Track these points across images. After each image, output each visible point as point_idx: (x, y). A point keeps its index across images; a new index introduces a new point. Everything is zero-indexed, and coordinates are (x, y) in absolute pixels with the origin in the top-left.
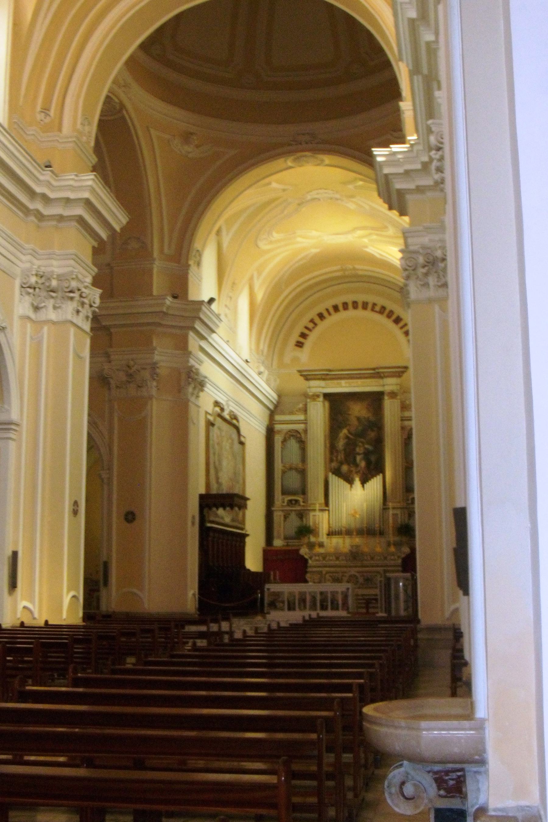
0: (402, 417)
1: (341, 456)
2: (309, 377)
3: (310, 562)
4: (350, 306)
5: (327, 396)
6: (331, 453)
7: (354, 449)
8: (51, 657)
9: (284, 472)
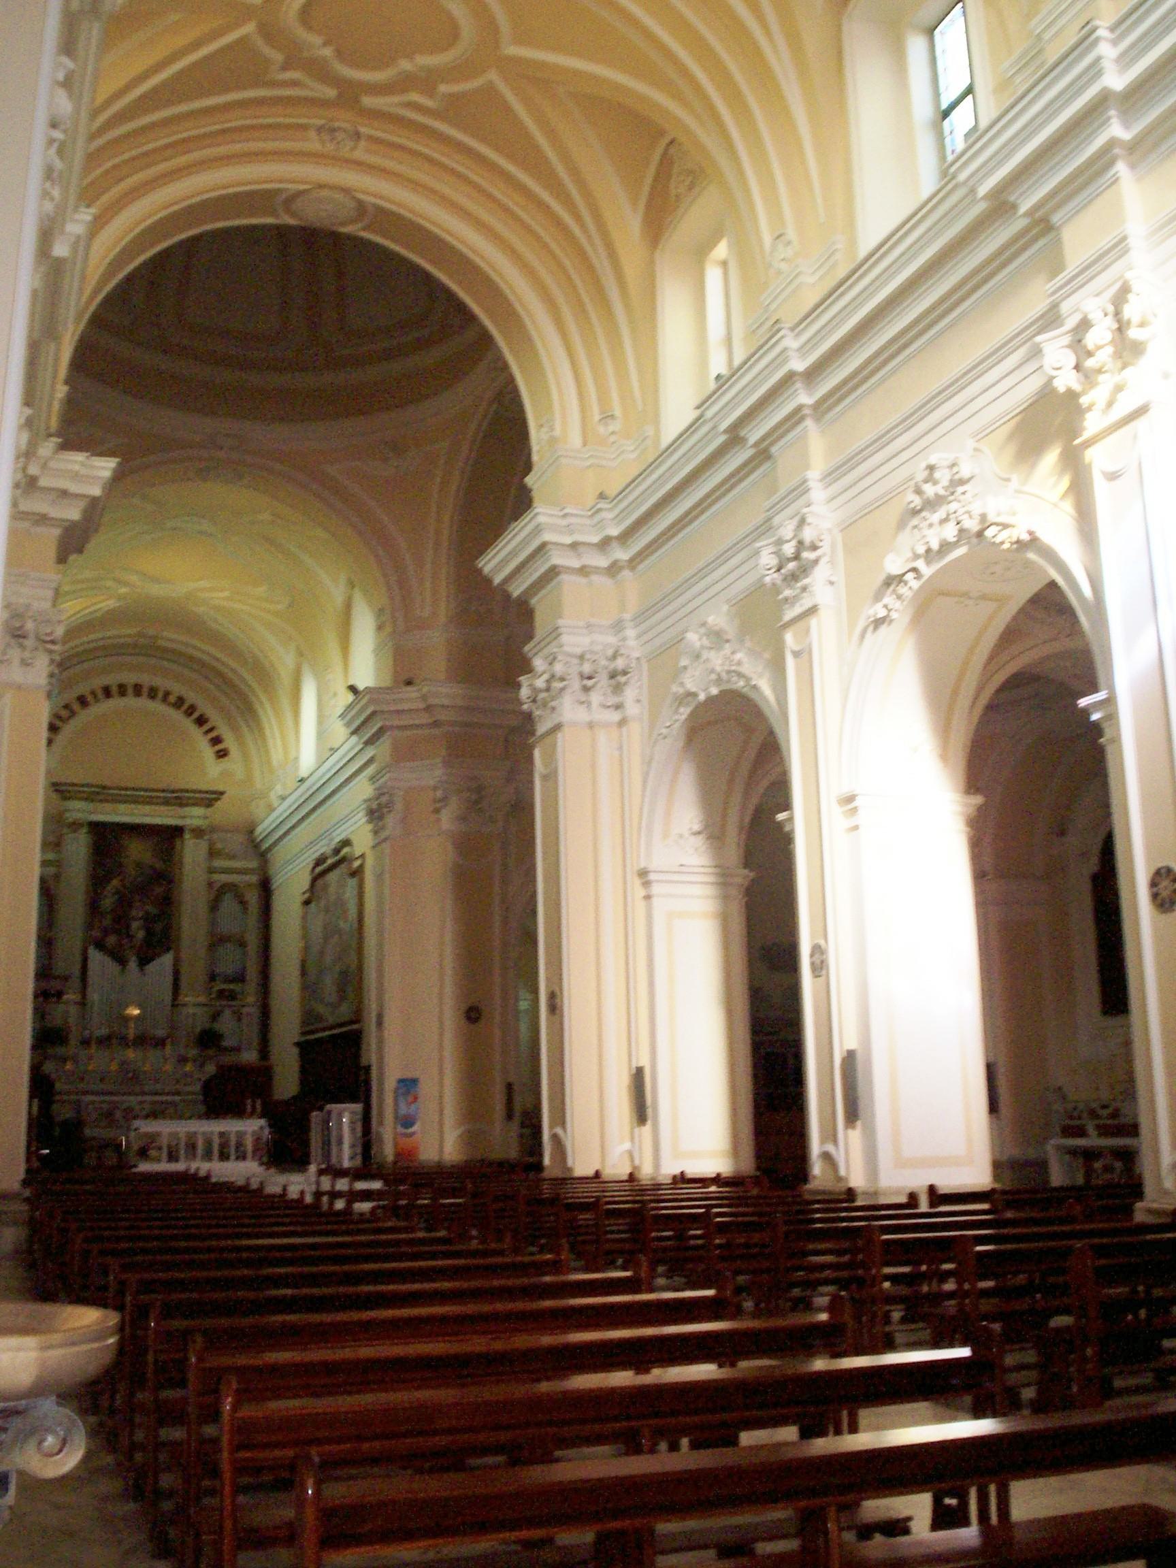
0: (209, 868)
1: (107, 922)
3: (58, 1086)
4: (130, 691)
8: (612, 1232)
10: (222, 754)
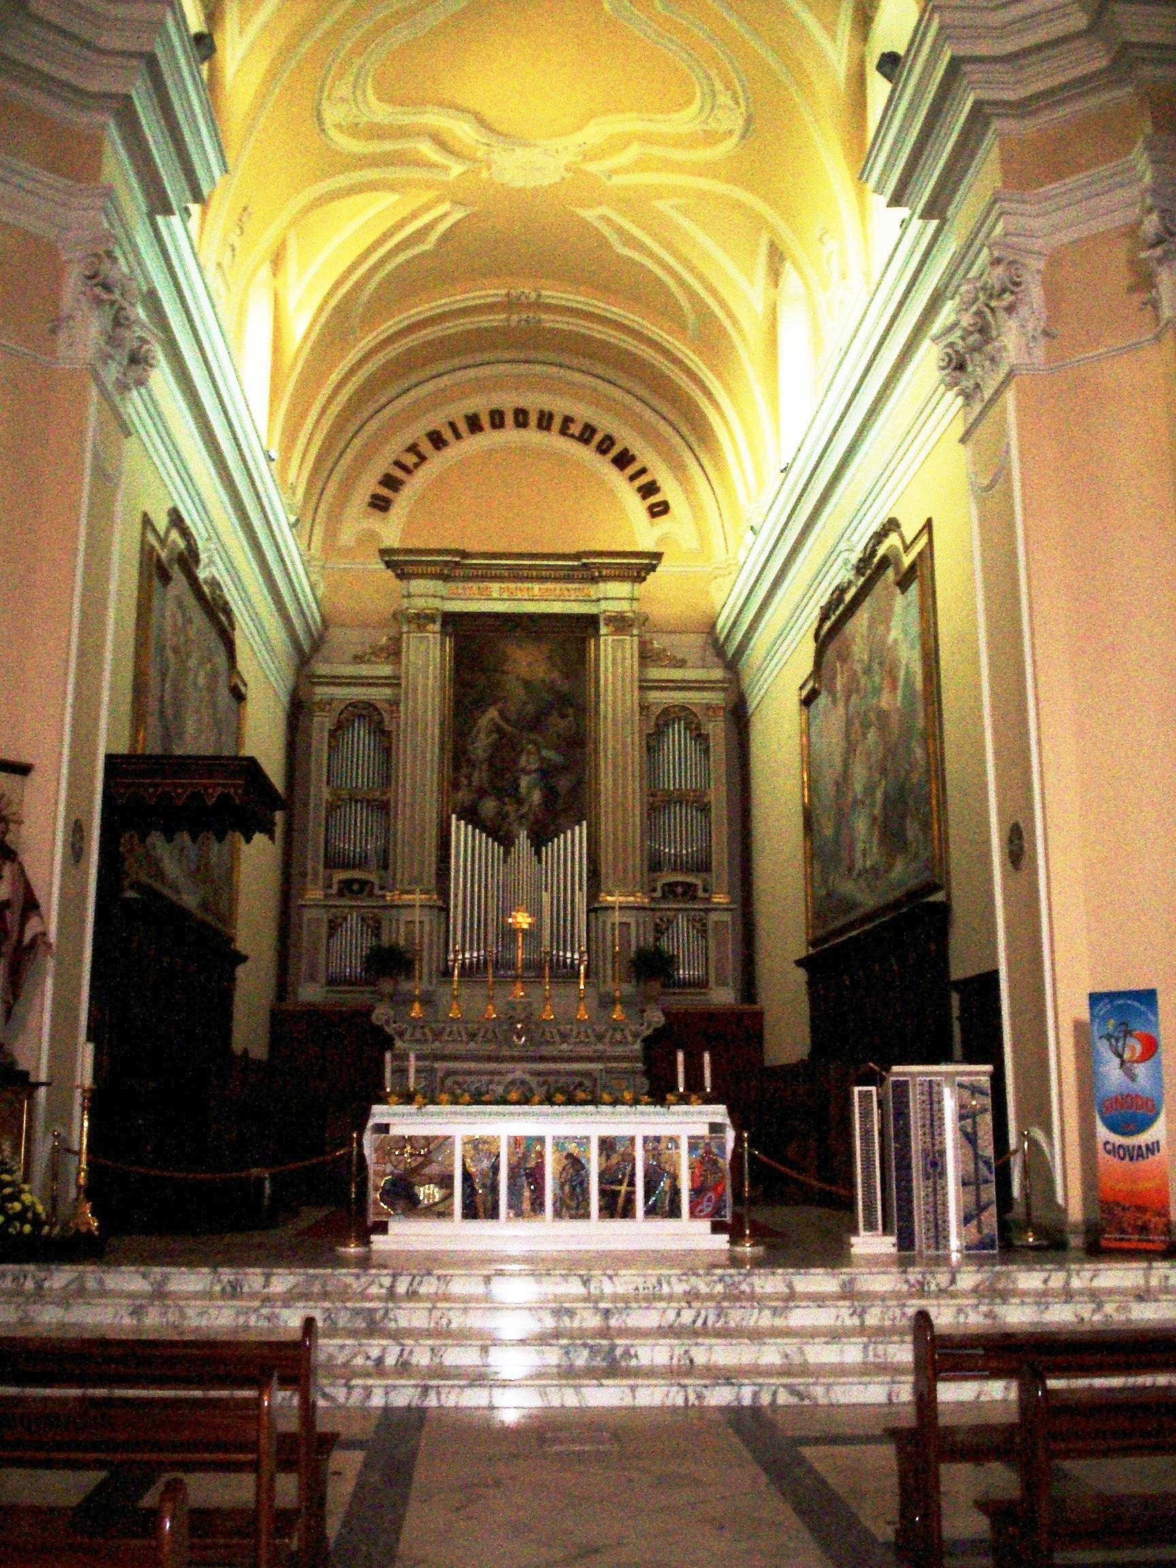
1: (480, 776)
2: (409, 569)
4: (509, 419)
5: (450, 619)
6: (457, 768)
7: (515, 761)
9: (332, 808)
10: (659, 510)
